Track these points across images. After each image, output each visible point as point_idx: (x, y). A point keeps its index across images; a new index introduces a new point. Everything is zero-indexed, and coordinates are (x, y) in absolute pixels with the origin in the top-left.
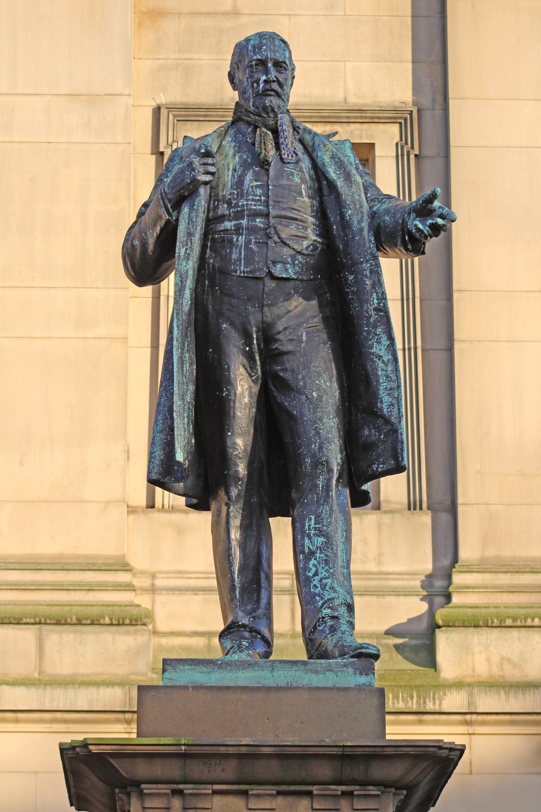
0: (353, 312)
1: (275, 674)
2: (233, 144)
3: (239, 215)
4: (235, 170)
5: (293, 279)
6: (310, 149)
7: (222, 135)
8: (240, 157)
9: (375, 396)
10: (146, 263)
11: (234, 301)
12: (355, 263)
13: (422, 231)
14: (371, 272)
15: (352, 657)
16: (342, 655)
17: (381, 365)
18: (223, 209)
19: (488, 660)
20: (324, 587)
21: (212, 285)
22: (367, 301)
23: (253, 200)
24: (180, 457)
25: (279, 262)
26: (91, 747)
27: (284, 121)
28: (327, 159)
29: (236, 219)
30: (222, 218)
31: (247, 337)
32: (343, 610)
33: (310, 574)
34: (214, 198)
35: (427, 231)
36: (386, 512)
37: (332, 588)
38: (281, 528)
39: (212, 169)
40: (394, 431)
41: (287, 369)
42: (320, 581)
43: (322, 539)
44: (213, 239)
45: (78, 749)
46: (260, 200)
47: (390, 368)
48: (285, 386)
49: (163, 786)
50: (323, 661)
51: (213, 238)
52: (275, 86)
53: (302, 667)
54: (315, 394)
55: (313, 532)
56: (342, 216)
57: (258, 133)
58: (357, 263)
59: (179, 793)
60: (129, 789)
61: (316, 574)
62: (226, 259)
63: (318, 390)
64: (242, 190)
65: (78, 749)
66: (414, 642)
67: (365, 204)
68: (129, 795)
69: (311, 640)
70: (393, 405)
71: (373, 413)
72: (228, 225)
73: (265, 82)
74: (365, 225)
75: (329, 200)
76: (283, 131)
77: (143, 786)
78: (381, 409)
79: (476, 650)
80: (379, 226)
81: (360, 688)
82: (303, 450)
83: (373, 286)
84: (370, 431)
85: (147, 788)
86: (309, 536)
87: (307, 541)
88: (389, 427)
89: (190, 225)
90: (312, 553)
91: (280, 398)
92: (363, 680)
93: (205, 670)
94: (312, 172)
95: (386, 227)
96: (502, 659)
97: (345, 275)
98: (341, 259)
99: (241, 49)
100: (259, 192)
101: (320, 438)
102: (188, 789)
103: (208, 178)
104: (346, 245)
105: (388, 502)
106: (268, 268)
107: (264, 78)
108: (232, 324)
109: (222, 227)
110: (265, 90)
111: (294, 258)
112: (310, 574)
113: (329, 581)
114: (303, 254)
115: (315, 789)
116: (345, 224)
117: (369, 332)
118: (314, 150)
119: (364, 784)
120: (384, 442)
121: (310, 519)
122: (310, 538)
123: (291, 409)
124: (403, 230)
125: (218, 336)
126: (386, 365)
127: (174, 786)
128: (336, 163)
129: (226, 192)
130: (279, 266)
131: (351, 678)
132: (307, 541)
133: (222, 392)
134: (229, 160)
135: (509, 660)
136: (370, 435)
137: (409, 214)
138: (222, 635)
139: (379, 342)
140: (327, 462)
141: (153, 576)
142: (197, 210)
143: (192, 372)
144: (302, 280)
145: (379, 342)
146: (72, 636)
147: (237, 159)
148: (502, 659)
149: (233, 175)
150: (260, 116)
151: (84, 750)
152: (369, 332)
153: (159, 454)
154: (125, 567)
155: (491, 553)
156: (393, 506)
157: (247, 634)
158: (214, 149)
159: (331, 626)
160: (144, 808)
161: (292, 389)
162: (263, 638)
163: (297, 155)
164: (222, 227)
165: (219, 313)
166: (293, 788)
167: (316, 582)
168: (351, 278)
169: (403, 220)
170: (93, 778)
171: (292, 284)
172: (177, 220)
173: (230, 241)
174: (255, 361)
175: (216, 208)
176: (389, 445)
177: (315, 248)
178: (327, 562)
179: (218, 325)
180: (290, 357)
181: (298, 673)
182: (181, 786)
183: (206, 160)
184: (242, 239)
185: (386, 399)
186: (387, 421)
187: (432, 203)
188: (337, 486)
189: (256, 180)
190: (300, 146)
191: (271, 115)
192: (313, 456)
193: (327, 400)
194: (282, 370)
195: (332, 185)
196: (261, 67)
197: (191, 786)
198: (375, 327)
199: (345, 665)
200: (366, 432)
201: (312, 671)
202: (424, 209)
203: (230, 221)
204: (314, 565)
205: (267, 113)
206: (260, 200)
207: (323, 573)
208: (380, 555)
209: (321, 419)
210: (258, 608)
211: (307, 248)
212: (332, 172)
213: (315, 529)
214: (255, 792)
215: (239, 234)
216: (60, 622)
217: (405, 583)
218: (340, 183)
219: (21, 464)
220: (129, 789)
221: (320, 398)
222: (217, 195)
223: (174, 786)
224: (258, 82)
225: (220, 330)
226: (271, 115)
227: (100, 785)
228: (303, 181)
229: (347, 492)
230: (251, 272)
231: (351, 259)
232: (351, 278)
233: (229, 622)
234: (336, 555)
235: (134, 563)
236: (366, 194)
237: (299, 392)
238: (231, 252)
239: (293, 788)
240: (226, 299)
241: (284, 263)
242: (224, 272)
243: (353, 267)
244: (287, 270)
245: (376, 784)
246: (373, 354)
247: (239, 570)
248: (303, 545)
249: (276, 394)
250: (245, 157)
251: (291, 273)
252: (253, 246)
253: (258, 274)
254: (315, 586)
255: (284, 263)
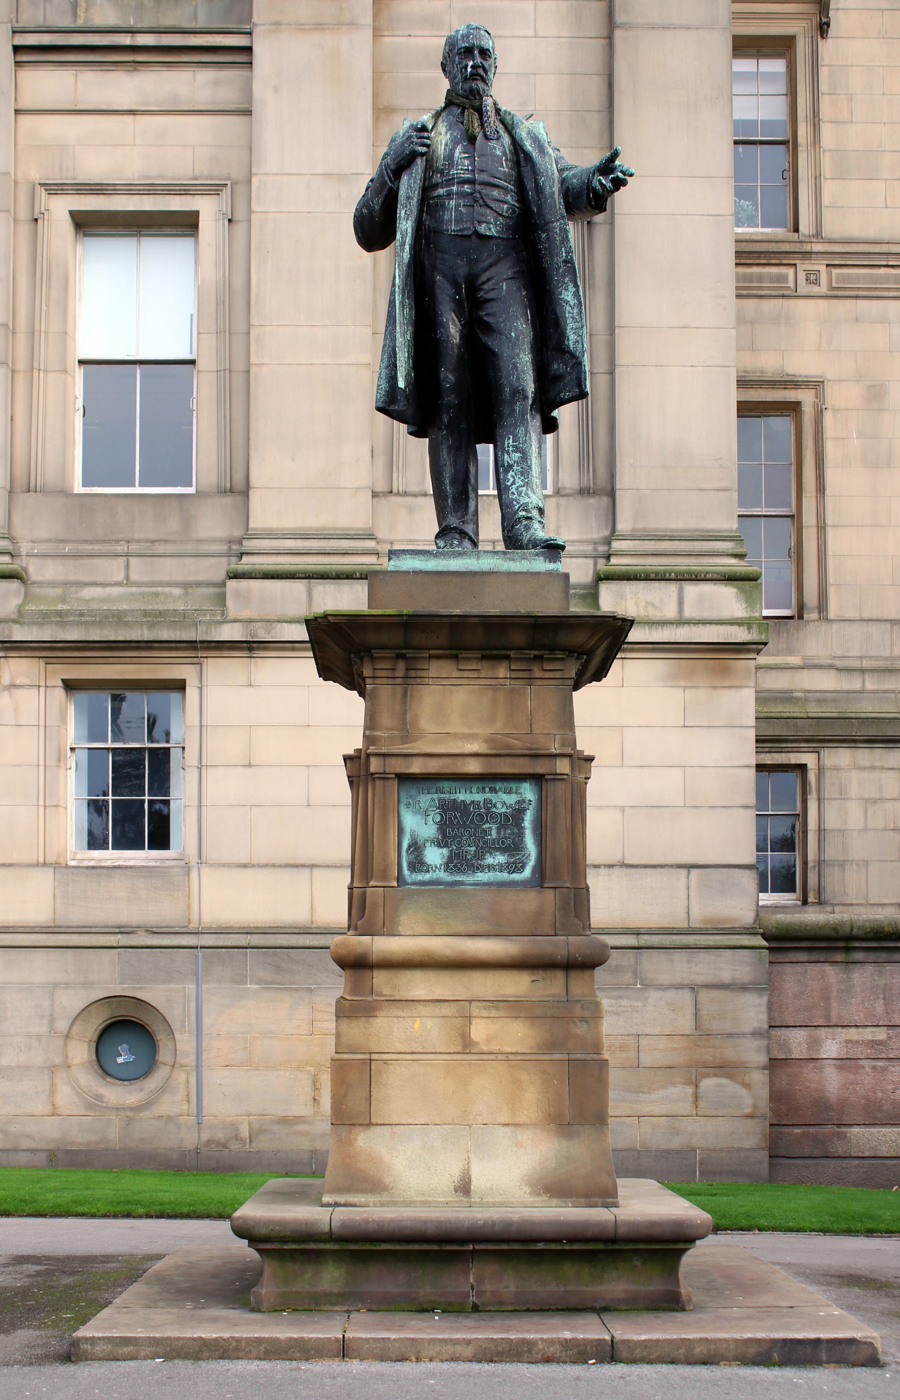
0: (545, 265)
1: (480, 561)
2: (445, 124)
3: (450, 182)
4: (446, 145)
5: (495, 237)
6: (510, 128)
7: (437, 115)
8: (451, 135)
9: (562, 336)
10: (373, 229)
11: (447, 257)
12: (547, 223)
13: (605, 186)
14: (561, 230)
15: (543, 548)
16: (534, 547)
17: (568, 308)
18: (437, 178)
19: (637, 604)
20: (520, 494)
21: (428, 244)
22: (557, 255)
23: (462, 169)
24: (401, 384)
25: (484, 222)
26: (330, 618)
27: (488, 102)
28: (524, 135)
29: (447, 186)
30: (436, 186)
31: (456, 285)
32: (535, 513)
33: (509, 484)
34: (429, 167)
35: (609, 185)
36: (562, 496)
37: (527, 494)
38: (486, 452)
39: (428, 142)
40: (579, 364)
41: (488, 314)
42: (517, 489)
43: (519, 455)
44: (428, 205)
45: (319, 620)
46: (468, 170)
47: (576, 311)
48: (488, 329)
49: (390, 651)
50: (519, 551)
51: (428, 204)
52: (481, 71)
53: (502, 556)
54: (513, 334)
55: (511, 449)
56: (537, 183)
57: (466, 113)
58: (549, 223)
59: (403, 657)
60: (362, 653)
61: (514, 483)
62: (440, 221)
63: (516, 331)
64: (453, 161)
65: (319, 620)
66: (582, 591)
67: (556, 172)
68: (362, 659)
69: (508, 537)
70: (577, 342)
71: (562, 350)
72: (441, 191)
73: (472, 67)
74: (556, 189)
75: (526, 171)
76: (487, 111)
77: (373, 651)
78: (568, 346)
79: (628, 597)
80: (568, 189)
81: (550, 574)
82: (504, 381)
83: (562, 242)
84: (559, 365)
85: (376, 653)
86: (508, 452)
87: (506, 456)
88: (574, 361)
89: (409, 187)
90: (510, 467)
91: (485, 339)
92: (551, 566)
93: (423, 558)
94: (511, 147)
95: (574, 189)
96: (647, 603)
97: (538, 234)
98: (536, 222)
99: (451, 43)
100: (466, 162)
101: (517, 371)
102: (410, 653)
103: (424, 149)
104: (540, 208)
105: (564, 488)
106: (474, 227)
107: (471, 63)
108: (444, 276)
109: (436, 193)
110: (472, 74)
111: (496, 220)
112: (509, 484)
113: (525, 489)
114: (503, 216)
115: (512, 653)
116: (539, 189)
117: (558, 281)
118: (513, 128)
119: (552, 649)
120: (570, 373)
121: (509, 439)
122: (508, 452)
123: (493, 347)
124: (588, 188)
125: (433, 286)
126: (572, 308)
127: (398, 651)
128: (532, 137)
129: (440, 163)
130: (484, 225)
131: (541, 565)
132: (506, 456)
133: (437, 334)
134: (442, 138)
135: (652, 604)
136: (559, 368)
137: (594, 174)
138: (438, 536)
139: (567, 290)
140: (523, 390)
141: (392, 543)
142: (415, 178)
143: (411, 316)
144: (502, 239)
145: (567, 290)
146: (332, 587)
147: (448, 135)
148: (647, 603)
149: (445, 149)
150: (467, 98)
151: (325, 620)
152: (558, 281)
153: (384, 386)
154: (371, 537)
155: (640, 525)
156: (568, 491)
157: (457, 536)
158: (430, 127)
159: (526, 525)
160: (375, 669)
161: (494, 331)
162: (471, 539)
163: (498, 132)
164: (436, 193)
165: (434, 267)
166: (495, 652)
167: (513, 490)
168: (544, 236)
169: (589, 180)
170: (334, 647)
171: (494, 241)
172: (398, 188)
173: (443, 205)
174: (464, 308)
175: (431, 178)
176: (574, 376)
177: (514, 212)
178: (522, 474)
179: (433, 278)
180: (492, 303)
181: (498, 561)
182: (404, 651)
183: (422, 134)
184: (453, 203)
185: (572, 337)
186: (573, 356)
187: (614, 162)
188: (531, 410)
189: (465, 153)
190: (501, 126)
191: (477, 97)
192: (511, 386)
193: (524, 338)
194: (486, 315)
195: (528, 157)
196: (468, 66)
197: (412, 651)
198: (564, 277)
199: (537, 555)
200: (556, 367)
201: (510, 559)
202: (607, 167)
203: (442, 188)
204: (512, 476)
205: (474, 96)
206: (468, 170)
207: (519, 482)
208: (558, 527)
209: (518, 355)
210: (466, 514)
211: (507, 212)
212: (528, 146)
213: (513, 446)
214: (463, 656)
215: (450, 199)
216: (323, 576)
217: (577, 548)
218: (535, 154)
219: (293, 460)
220: (362, 653)
221: (517, 337)
222: (432, 167)
223: (398, 651)
224: (466, 67)
225: (434, 282)
226: (477, 97)
227: (339, 651)
228: (504, 153)
229: (538, 417)
230: (460, 230)
231: (544, 219)
232: (544, 236)
233: (444, 525)
234: (530, 467)
235: (380, 535)
236: (557, 165)
237: (500, 333)
238: (444, 215)
239: (495, 652)
240: (439, 255)
241: (488, 223)
242: (438, 232)
243: (545, 226)
244: (490, 229)
245: (563, 649)
246: (561, 299)
247: (450, 483)
248: (503, 460)
249: (481, 336)
250: (455, 134)
251: (493, 232)
252: (461, 209)
253: (466, 233)
254: (513, 493)
255: (488, 223)
